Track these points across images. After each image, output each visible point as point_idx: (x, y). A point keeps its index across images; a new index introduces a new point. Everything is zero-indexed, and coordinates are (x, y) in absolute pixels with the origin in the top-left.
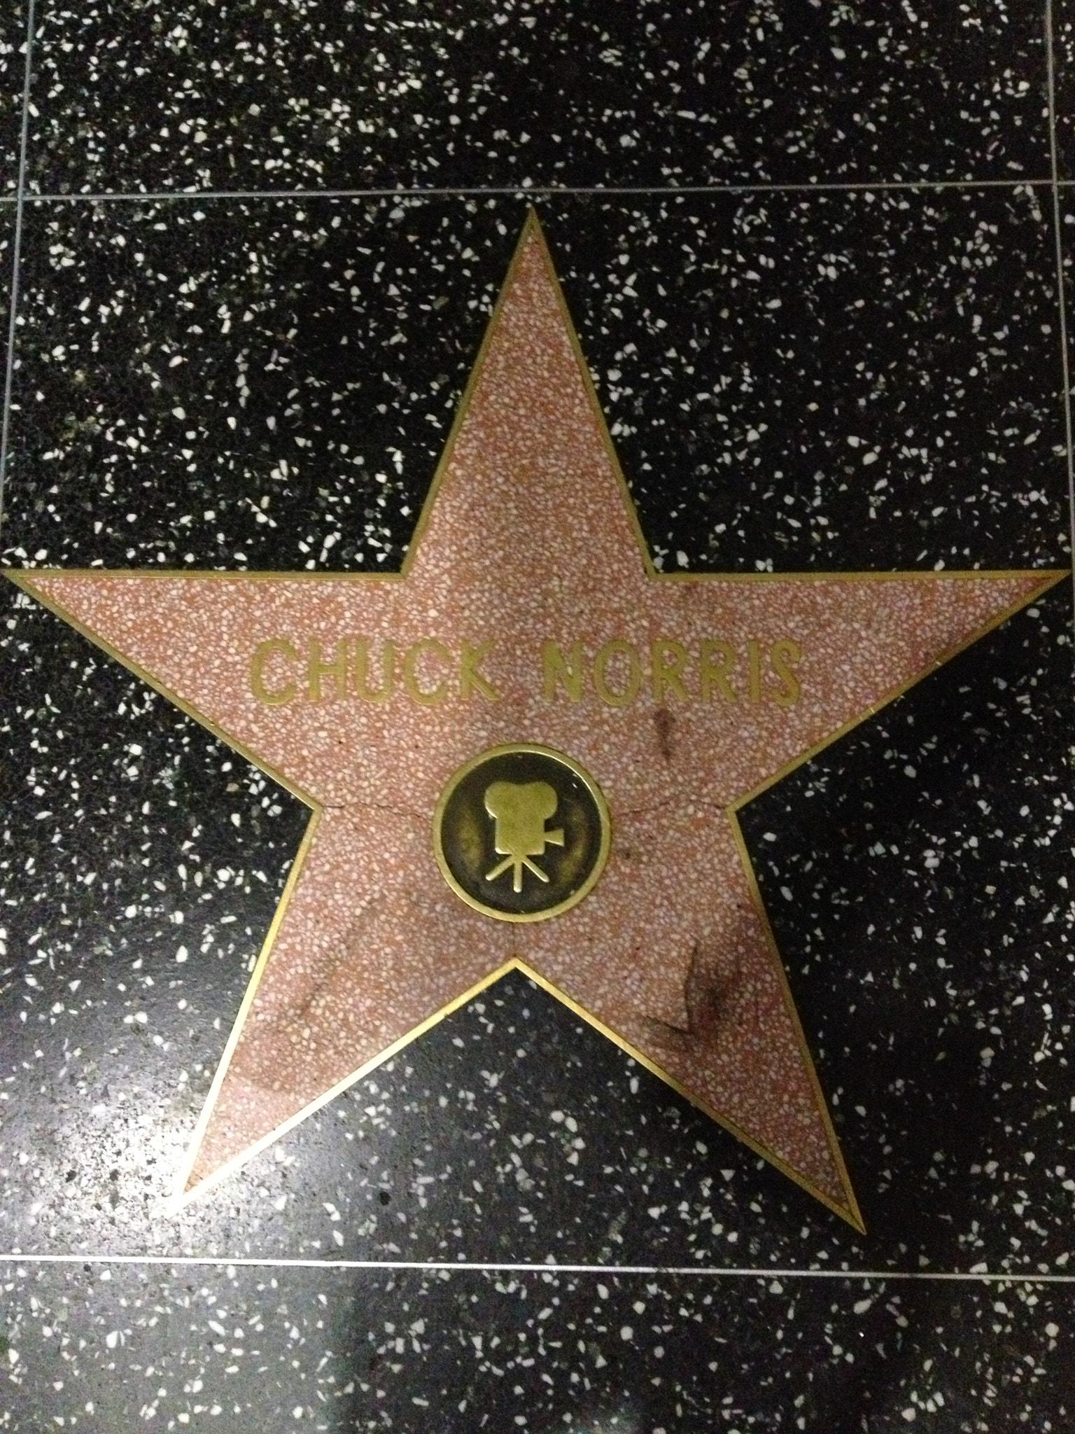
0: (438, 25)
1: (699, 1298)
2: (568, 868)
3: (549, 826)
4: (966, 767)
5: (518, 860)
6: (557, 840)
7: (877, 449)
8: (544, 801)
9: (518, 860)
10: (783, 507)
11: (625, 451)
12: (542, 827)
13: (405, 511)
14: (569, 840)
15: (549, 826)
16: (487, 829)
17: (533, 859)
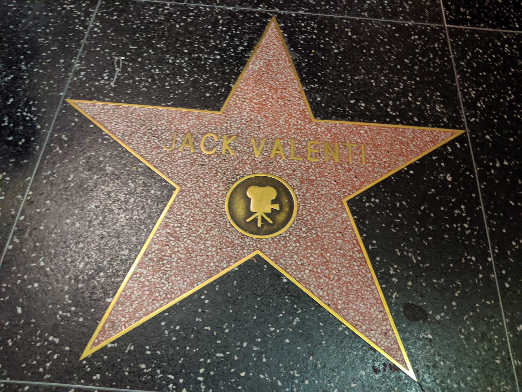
0: (488, 302)
1: (369, 51)
2: (281, 217)
3: (273, 202)
4: (430, 238)
5: (259, 215)
6: (276, 207)
7: (51, 362)
8: (272, 193)
9: (259, 215)
10: (83, 16)
11: (296, 69)
12: (270, 202)
13: (474, 136)
14: (281, 207)
15: (273, 202)
16: (248, 200)
17: (267, 214)
